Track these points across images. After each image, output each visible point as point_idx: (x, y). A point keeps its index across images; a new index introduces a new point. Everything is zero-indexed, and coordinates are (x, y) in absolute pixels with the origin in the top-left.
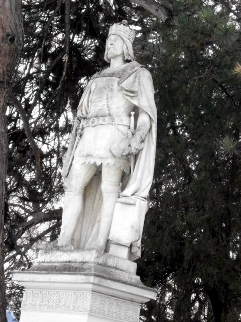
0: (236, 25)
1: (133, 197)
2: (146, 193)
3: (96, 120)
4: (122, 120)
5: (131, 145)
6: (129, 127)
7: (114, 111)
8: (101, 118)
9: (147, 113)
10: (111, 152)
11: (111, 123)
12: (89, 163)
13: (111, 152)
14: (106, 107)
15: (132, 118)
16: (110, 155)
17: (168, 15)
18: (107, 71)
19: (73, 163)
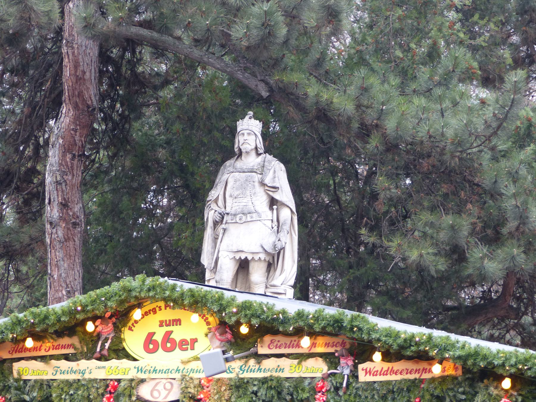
0: (432, 152)
1: (283, 286)
2: (292, 282)
3: (244, 217)
4: (267, 216)
5: (281, 239)
6: (272, 220)
7: (258, 209)
8: (248, 215)
9: (288, 206)
10: (262, 247)
11: (259, 219)
12: (240, 258)
13: (262, 247)
14: (251, 204)
15: (275, 211)
16: (261, 250)
17: (269, 91)
18: (239, 164)
19: (220, 255)
